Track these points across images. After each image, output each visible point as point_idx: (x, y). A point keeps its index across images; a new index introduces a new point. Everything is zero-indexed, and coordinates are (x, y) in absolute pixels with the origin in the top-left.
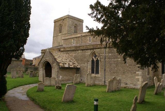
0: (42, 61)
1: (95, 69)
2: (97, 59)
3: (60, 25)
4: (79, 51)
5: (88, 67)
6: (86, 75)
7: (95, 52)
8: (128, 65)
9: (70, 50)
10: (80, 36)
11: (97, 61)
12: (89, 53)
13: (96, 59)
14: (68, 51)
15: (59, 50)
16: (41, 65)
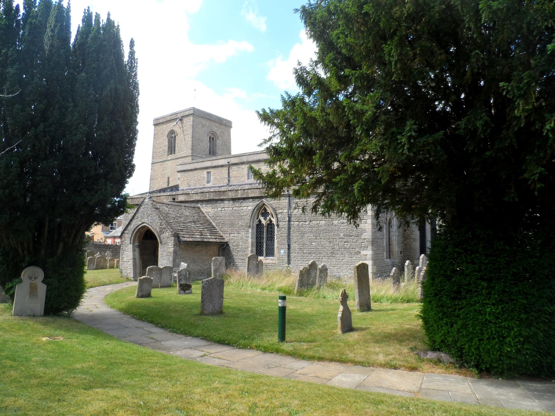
0: (132, 227)
1: (265, 246)
2: (271, 221)
3: (172, 132)
4: (226, 202)
5: (247, 240)
6: (247, 260)
7: (264, 204)
8: (342, 235)
9: (202, 198)
10: (226, 163)
11: (270, 225)
12: (250, 206)
13: (269, 222)
14: (198, 201)
15: (174, 199)
16: (128, 236)
